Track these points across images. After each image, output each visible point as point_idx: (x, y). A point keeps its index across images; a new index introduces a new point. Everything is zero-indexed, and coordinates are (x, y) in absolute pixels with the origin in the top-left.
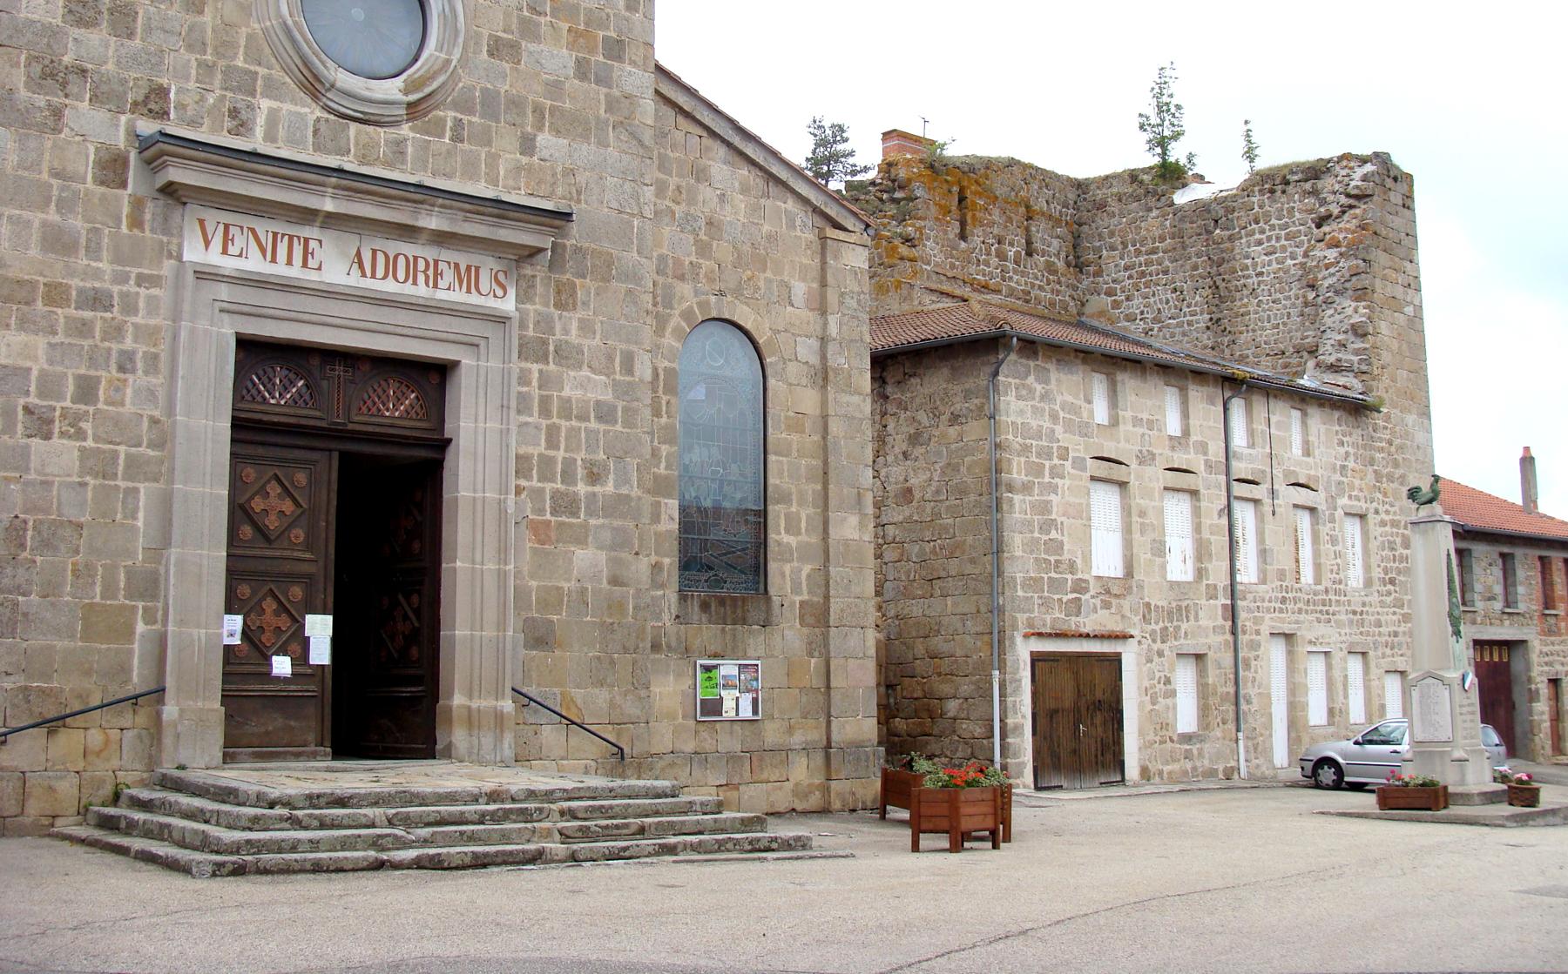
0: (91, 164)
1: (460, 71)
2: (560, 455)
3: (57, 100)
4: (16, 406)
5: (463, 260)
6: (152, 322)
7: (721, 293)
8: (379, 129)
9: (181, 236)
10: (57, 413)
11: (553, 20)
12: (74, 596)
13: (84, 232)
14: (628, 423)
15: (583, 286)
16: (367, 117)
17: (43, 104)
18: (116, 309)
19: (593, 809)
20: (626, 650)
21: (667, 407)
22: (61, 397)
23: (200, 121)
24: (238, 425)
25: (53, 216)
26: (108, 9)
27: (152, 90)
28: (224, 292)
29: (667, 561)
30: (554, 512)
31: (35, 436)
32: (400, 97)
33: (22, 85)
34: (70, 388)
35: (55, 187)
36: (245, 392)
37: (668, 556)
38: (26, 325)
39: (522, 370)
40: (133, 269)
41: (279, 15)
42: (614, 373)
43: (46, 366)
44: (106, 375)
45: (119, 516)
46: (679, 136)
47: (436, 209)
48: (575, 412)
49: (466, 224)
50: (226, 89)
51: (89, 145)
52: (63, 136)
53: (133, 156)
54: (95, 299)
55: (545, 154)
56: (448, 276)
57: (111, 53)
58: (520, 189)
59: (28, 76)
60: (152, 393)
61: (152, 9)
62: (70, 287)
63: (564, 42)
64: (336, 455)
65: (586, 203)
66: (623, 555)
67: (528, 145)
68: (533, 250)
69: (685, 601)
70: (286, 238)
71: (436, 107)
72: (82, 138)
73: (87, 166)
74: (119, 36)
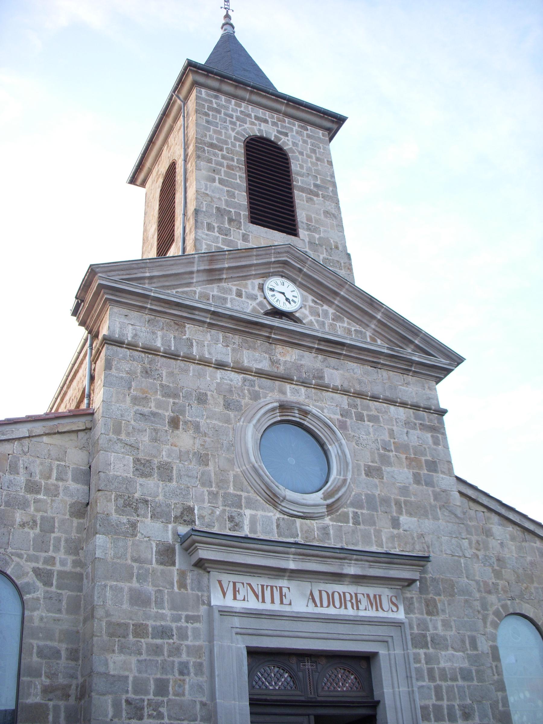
0: (154, 553)
1: (352, 485)
3: (134, 518)
4: (121, 700)
5: (372, 591)
6: (197, 643)
7: (513, 599)
8: (312, 521)
9: (209, 591)
10: (146, 703)
11: (397, 454)
13: (153, 593)
14: (480, 680)
15: (440, 601)
16: (305, 515)
17: (125, 521)
18: (175, 637)
21: (496, 669)
22: (147, 693)
23: (213, 524)
24: (254, 703)
25: (135, 584)
26: (157, 467)
27: (184, 509)
28: (236, 622)
31: (133, 718)
32: (322, 502)
33: (113, 511)
34: (152, 687)
35: (135, 567)
36: (254, 683)
38: (124, 650)
40: (183, 613)
41: (250, 462)
42: (467, 650)
43: (137, 674)
44: (173, 677)
46: (472, 513)
47: (353, 562)
48: (449, 676)
49: (371, 570)
50: (225, 506)
51: (152, 542)
52: (137, 538)
53: (177, 547)
54: (162, 632)
55: (406, 527)
56: (364, 602)
57: (160, 490)
58: (396, 548)
59: (117, 506)
60: (200, 687)
61: (180, 465)
62: (148, 625)
63: (405, 464)
64: (312, 718)
65: (433, 552)
67: (395, 523)
68: (410, 581)
70: (269, 588)
71: (342, 507)
72: (148, 539)
73: (152, 554)
74: (164, 481)
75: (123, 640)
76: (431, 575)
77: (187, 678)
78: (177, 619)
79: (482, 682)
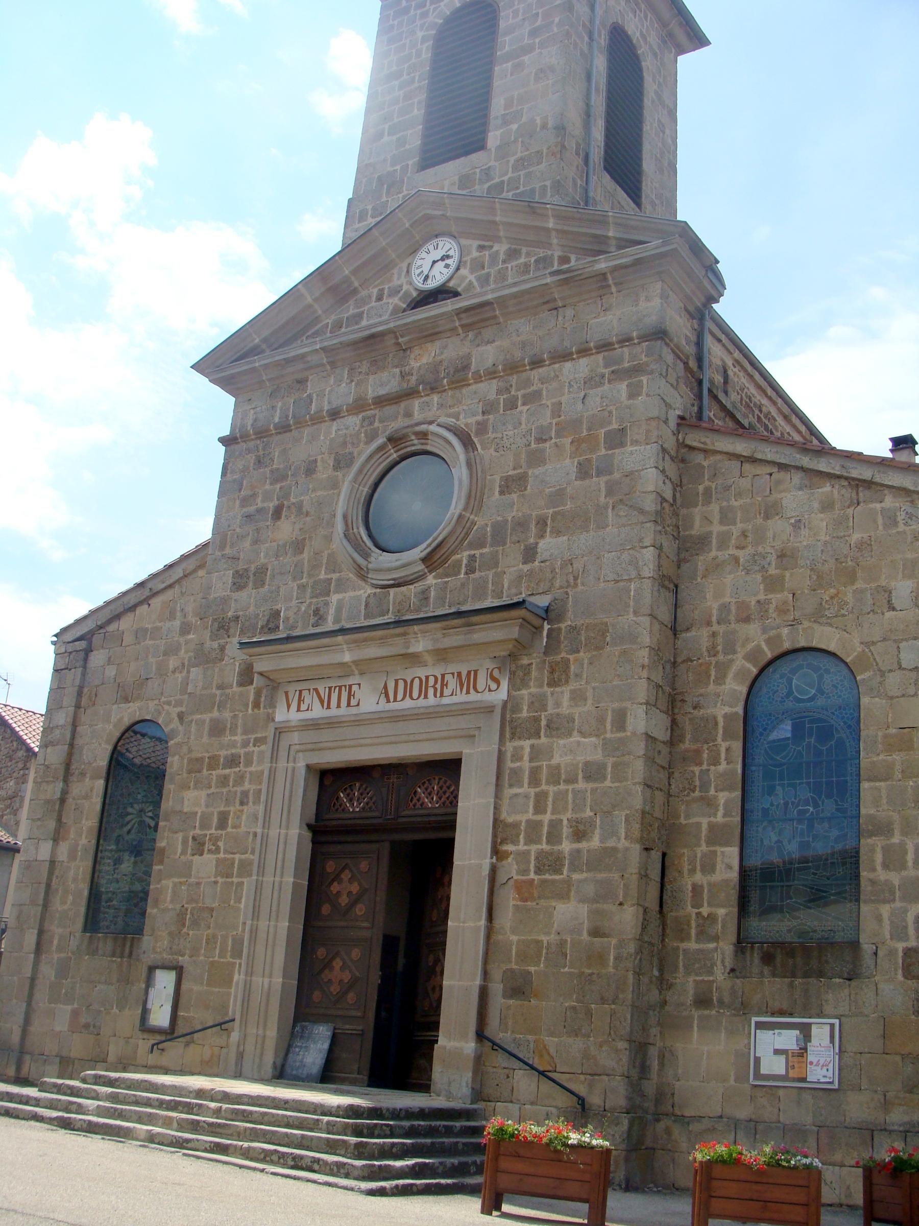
2: (546, 818)
12: (205, 956)
13: (229, 719)
19: (236, 1111)
20: (603, 1000)
22: (209, 828)
29: (721, 912)
30: (538, 871)
37: (723, 906)
39: (515, 748)
45: (232, 902)
48: (563, 777)
55: (546, 555)
56: (452, 683)
64: (387, 845)
65: (583, 584)
66: (605, 906)
67: (530, 554)
69: (743, 953)
75: (197, 774)
76: (569, 623)
77: (245, 808)
78: (245, 744)
79: (620, 782)
